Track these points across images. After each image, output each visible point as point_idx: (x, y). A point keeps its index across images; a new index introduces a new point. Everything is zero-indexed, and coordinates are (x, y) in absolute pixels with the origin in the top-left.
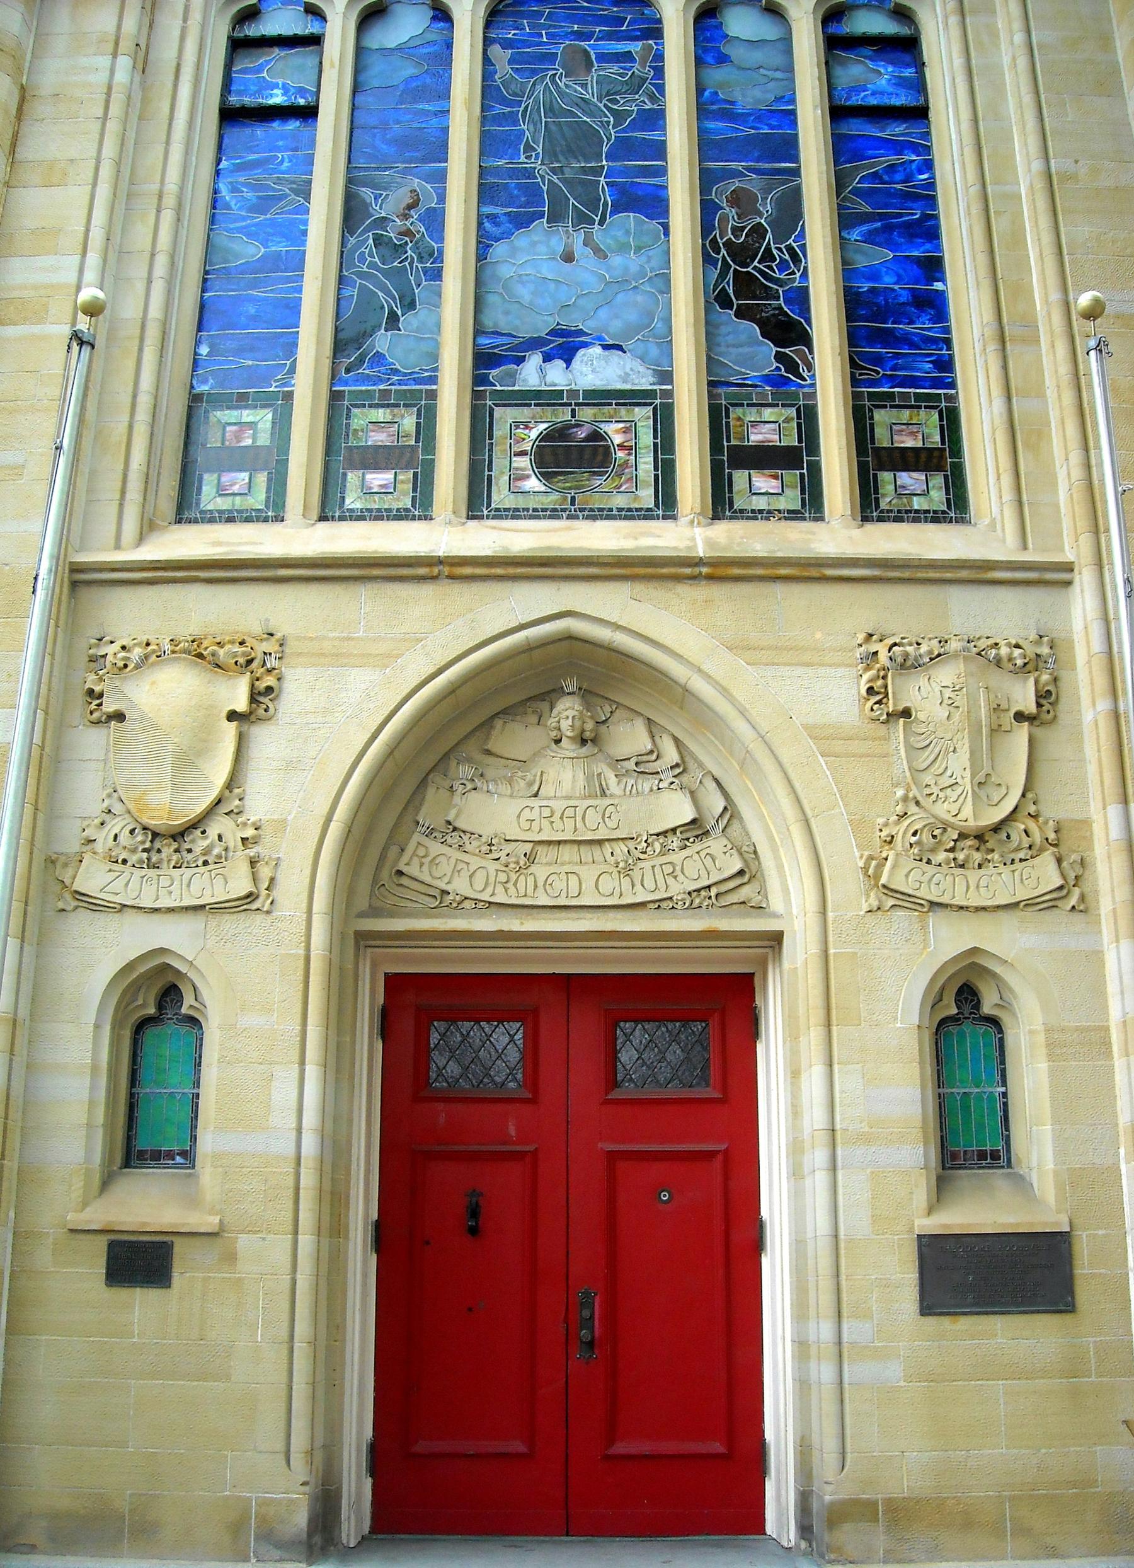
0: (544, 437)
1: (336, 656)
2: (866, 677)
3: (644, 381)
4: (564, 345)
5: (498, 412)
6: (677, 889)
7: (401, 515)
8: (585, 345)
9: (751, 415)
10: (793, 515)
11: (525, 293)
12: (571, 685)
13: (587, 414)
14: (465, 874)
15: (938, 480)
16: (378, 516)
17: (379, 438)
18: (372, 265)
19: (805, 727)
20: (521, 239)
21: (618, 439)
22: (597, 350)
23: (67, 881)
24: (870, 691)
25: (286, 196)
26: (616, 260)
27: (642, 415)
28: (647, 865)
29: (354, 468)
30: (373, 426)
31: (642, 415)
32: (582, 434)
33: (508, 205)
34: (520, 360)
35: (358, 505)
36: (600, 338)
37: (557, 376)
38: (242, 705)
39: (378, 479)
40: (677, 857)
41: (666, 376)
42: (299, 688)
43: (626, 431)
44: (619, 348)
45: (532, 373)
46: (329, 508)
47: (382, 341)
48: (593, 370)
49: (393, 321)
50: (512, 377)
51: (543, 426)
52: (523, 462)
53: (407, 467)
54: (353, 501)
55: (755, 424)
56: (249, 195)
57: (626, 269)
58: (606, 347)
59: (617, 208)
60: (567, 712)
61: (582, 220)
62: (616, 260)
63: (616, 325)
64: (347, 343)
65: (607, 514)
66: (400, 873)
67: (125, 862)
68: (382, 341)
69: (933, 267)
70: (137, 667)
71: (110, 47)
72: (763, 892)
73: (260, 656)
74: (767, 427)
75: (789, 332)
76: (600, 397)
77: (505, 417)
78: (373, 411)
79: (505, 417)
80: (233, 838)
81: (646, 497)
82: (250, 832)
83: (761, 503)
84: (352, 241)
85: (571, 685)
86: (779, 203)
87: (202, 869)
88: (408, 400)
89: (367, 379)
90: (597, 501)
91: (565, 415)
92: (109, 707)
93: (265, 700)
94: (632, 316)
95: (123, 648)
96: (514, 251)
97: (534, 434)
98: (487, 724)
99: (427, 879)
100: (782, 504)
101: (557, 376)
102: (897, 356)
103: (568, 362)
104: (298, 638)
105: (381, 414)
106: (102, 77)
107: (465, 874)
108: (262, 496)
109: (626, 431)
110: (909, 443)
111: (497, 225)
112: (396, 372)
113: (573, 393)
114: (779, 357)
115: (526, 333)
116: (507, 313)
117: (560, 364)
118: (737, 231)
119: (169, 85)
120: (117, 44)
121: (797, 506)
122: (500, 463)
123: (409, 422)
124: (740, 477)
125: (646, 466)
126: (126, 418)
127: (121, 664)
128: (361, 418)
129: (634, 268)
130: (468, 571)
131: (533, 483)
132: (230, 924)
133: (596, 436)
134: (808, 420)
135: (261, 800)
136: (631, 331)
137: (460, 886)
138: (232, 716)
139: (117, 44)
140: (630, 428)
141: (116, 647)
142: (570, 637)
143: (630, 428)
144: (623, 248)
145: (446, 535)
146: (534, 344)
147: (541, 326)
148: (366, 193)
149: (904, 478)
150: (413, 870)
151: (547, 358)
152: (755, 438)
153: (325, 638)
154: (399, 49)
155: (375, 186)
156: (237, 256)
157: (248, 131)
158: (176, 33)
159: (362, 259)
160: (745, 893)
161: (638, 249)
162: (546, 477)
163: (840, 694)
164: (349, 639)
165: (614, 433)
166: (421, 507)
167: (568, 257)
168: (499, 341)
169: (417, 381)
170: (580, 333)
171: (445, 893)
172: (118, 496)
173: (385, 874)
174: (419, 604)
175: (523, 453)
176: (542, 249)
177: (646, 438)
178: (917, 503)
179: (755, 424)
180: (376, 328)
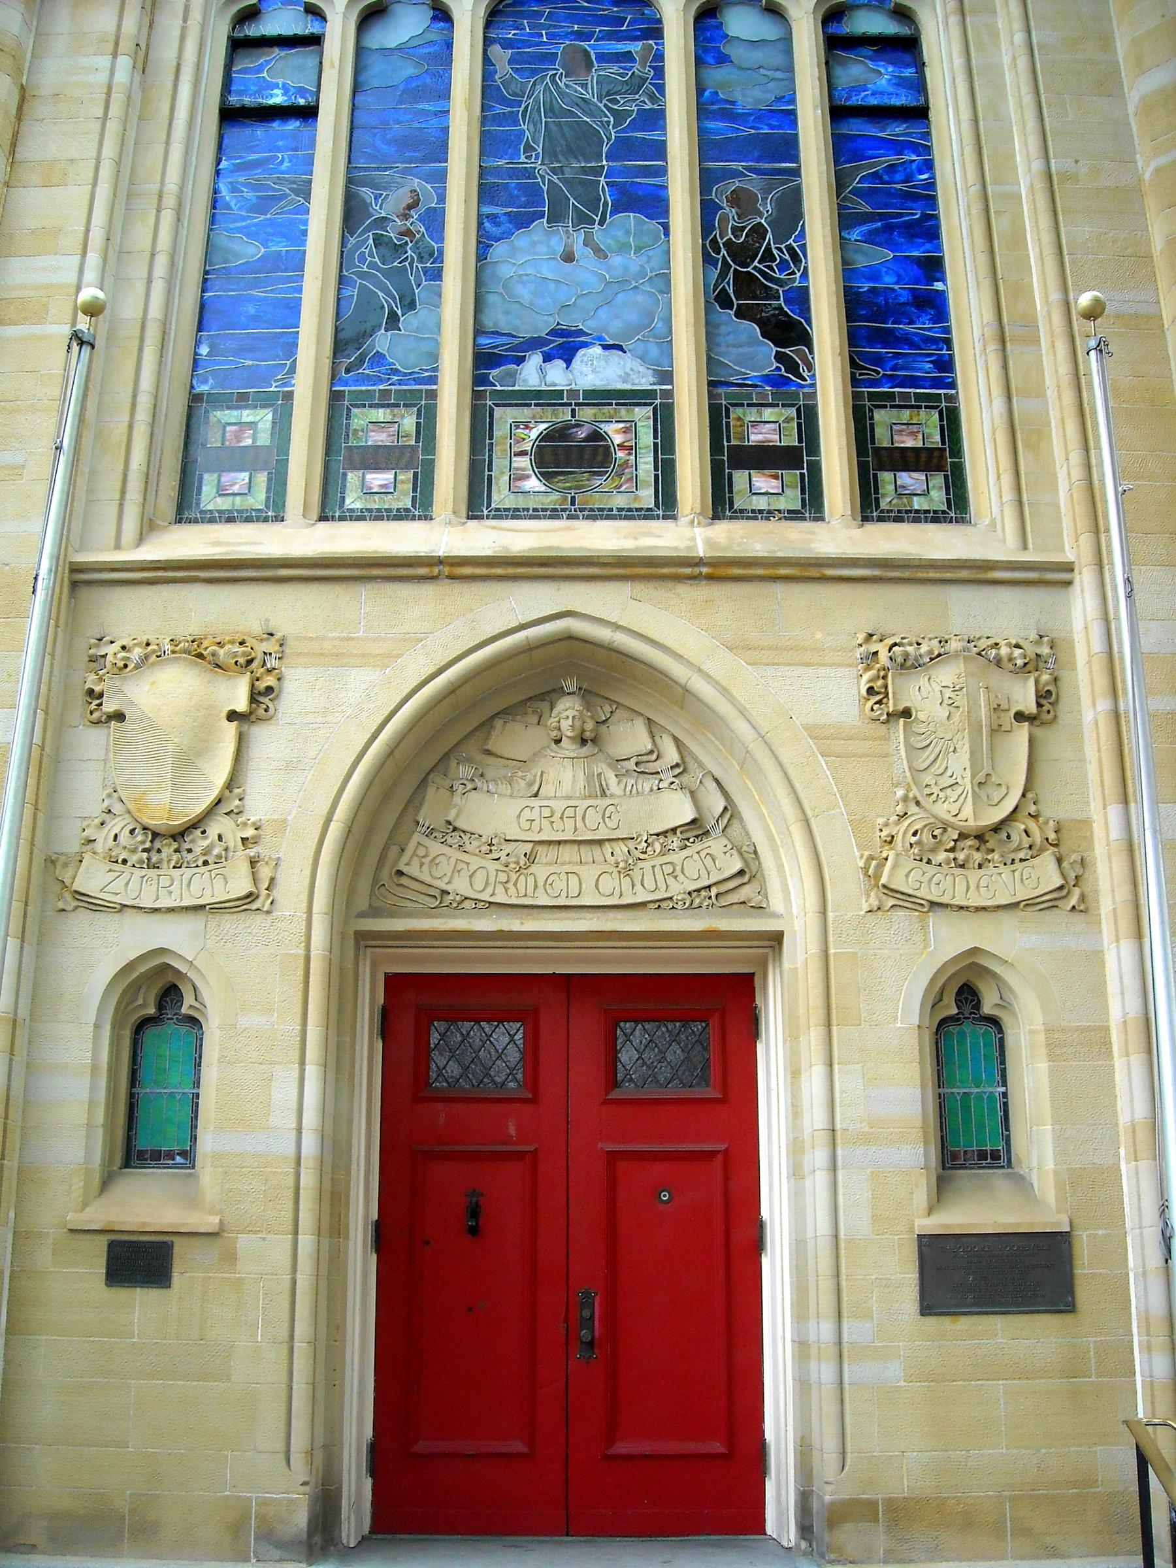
0: (544, 437)
1: (337, 657)
2: (866, 677)
3: (644, 381)
4: (564, 345)
5: (498, 412)
6: (677, 889)
7: (401, 515)
8: (585, 345)
9: (751, 415)
10: (794, 515)
11: (525, 293)
12: (571, 685)
13: (586, 414)
14: (465, 874)
15: (938, 480)
16: (379, 516)
17: (379, 438)
18: (372, 265)
19: (806, 727)
20: (521, 239)
21: (618, 439)
22: (597, 350)
23: (67, 881)
24: (871, 691)
25: (286, 196)
26: (616, 260)
27: (642, 415)
28: (647, 865)
29: (353, 467)
30: (373, 425)
31: (642, 415)
32: (582, 434)
33: (508, 202)
34: (520, 360)
35: (358, 505)
36: (600, 338)
37: (557, 376)
38: (242, 705)
39: (378, 479)
40: (677, 857)
41: (666, 376)
42: (299, 689)
43: (626, 431)
44: (619, 348)
45: (533, 373)
46: (329, 508)
47: (382, 341)
48: (593, 370)
49: (393, 321)
50: (513, 376)
51: (543, 426)
52: (523, 462)
53: (407, 467)
54: (353, 501)
55: (755, 424)
56: (248, 194)
57: (626, 268)
58: (606, 347)
59: (616, 209)
60: (567, 712)
61: (583, 220)
62: (616, 260)
63: (616, 325)
64: (347, 343)
65: (595, 515)
66: (400, 873)
67: (125, 862)
68: (382, 341)
69: (933, 267)
70: (137, 667)
71: (110, 47)
72: (763, 892)
73: (260, 656)
74: (767, 427)
75: (789, 332)
76: (600, 397)
77: (505, 417)
78: (373, 411)
79: (505, 417)
80: (233, 837)
81: (647, 497)
82: (250, 832)
83: (761, 503)
84: (352, 241)
85: (571, 685)
86: (780, 203)
87: (202, 869)
88: (408, 400)
89: (367, 379)
90: (597, 502)
91: (565, 415)
92: (109, 707)
93: (265, 700)
94: (633, 316)
95: (124, 648)
96: (514, 251)
97: (534, 434)
98: (487, 725)
99: (427, 878)
100: (782, 504)
101: (557, 376)
102: (897, 356)
103: (568, 362)
104: (298, 638)
105: (381, 414)
106: (102, 77)
107: (465, 874)
108: (263, 496)
109: (626, 431)
110: (910, 443)
111: (497, 224)
112: (395, 372)
113: (573, 393)
114: (780, 357)
115: (526, 333)
116: (507, 313)
117: (560, 364)
118: (737, 231)
119: (169, 85)
120: (117, 44)
121: (797, 506)
122: (500, 462)
123: (409, 422)
124: (740, 478)
125: (646, 465)
126: (126, 418)
127: (121, 664)
128: (361, 418)
129: (634, 268)
130: (468, 571)
131: (533, 483)
132: (229, 923)
133: (596, 436)
134: (808, 420)
135: (262, 799)
136: (631, 331)
137: (460, 886)
138: (232, 716)
139: (117, 44)
140: (630, 428)
141: (116, 647)
142: (570, 638)
143: (630, 428)
144: (623, 248)
145: (446, 535)
146: (534, 343)
147: (541, 326)
148: (367, 193)
149: (905, 478)
150: (413, 870)
151: (547, 358)
152: (756, 438)
153: (324, 638)
154: (399, 48)
155: (374, 186)
156: (237, 256)
157: (248, 131)
158: (176, 33)
159: (362, 259)
160: (745, 893)
161: (638, 249)
162: (547, 477)
163: (840, 694)
164: (349, 639)
165: (615, 433)
166: (421, 506)
167: (569, 257)
168: (499, 340)
169: (418, 381)
170: (581, 333)
171: (445, 893)
172: (118, 497)
173: (385, 874)
174: (419, 603)
175: (523, 453)
176: (543, 249)
177: (646, 438)
178: (918, 503)
179: (755, 424)
180: (375, 328)
